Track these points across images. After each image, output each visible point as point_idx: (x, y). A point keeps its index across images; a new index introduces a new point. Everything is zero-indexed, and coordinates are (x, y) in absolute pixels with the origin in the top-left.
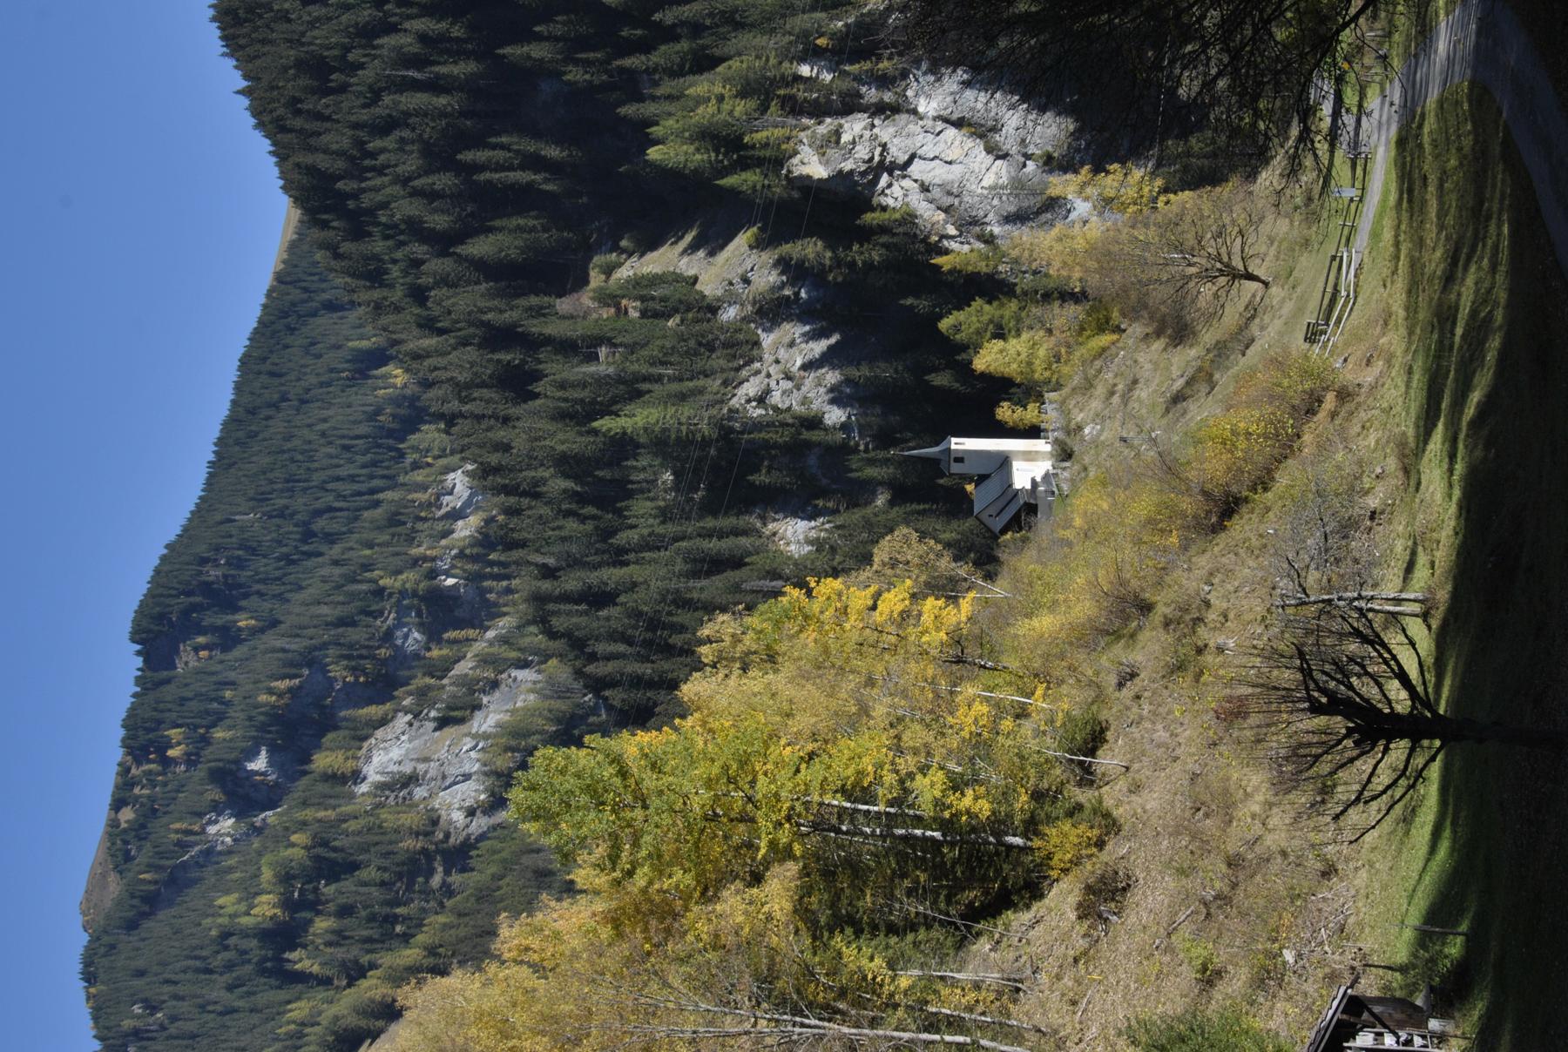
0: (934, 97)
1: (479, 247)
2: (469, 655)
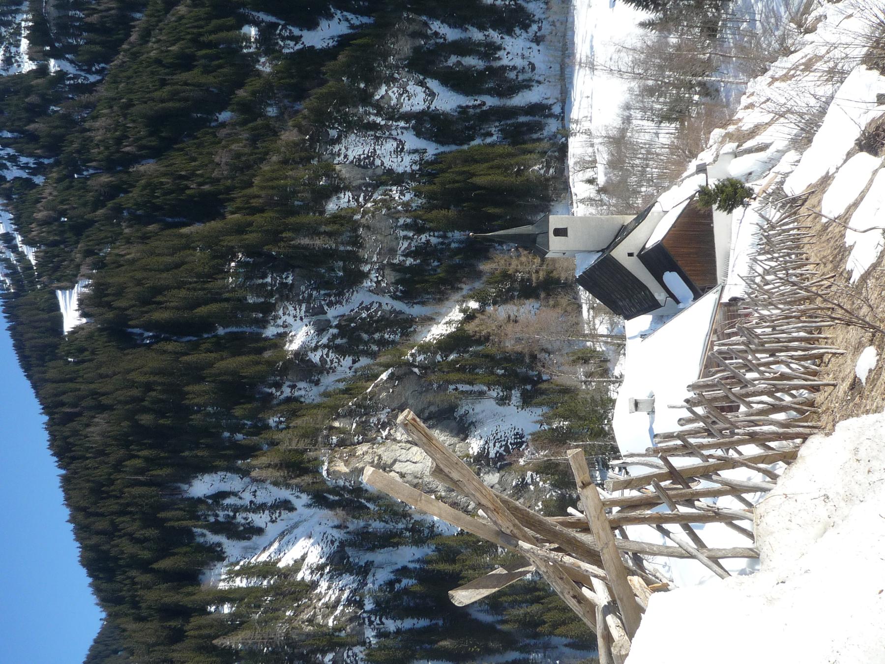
1: (165, 564)
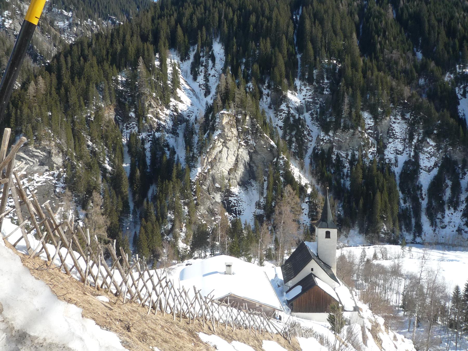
0: (244, 155)
1: (180, 31)
2: (56, 32)
